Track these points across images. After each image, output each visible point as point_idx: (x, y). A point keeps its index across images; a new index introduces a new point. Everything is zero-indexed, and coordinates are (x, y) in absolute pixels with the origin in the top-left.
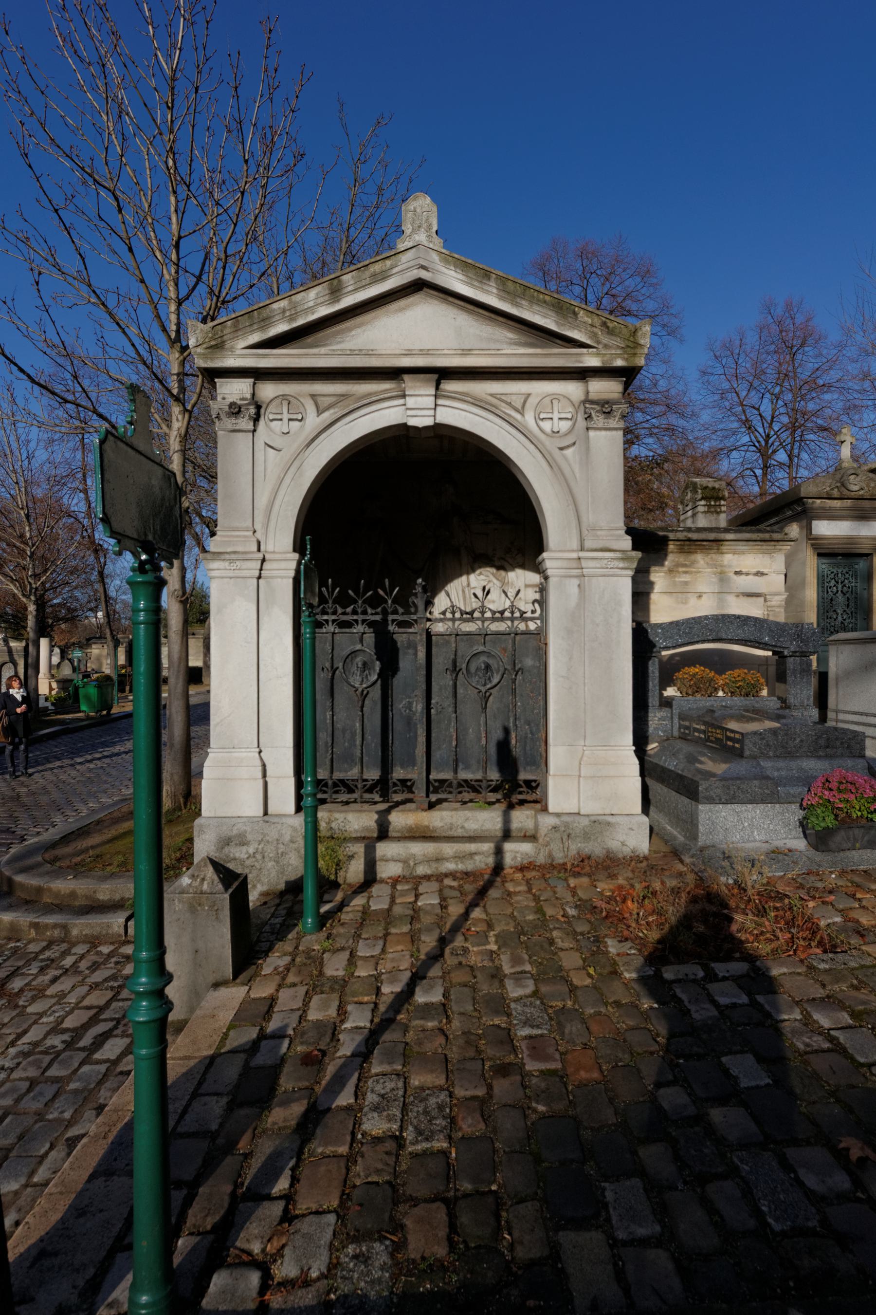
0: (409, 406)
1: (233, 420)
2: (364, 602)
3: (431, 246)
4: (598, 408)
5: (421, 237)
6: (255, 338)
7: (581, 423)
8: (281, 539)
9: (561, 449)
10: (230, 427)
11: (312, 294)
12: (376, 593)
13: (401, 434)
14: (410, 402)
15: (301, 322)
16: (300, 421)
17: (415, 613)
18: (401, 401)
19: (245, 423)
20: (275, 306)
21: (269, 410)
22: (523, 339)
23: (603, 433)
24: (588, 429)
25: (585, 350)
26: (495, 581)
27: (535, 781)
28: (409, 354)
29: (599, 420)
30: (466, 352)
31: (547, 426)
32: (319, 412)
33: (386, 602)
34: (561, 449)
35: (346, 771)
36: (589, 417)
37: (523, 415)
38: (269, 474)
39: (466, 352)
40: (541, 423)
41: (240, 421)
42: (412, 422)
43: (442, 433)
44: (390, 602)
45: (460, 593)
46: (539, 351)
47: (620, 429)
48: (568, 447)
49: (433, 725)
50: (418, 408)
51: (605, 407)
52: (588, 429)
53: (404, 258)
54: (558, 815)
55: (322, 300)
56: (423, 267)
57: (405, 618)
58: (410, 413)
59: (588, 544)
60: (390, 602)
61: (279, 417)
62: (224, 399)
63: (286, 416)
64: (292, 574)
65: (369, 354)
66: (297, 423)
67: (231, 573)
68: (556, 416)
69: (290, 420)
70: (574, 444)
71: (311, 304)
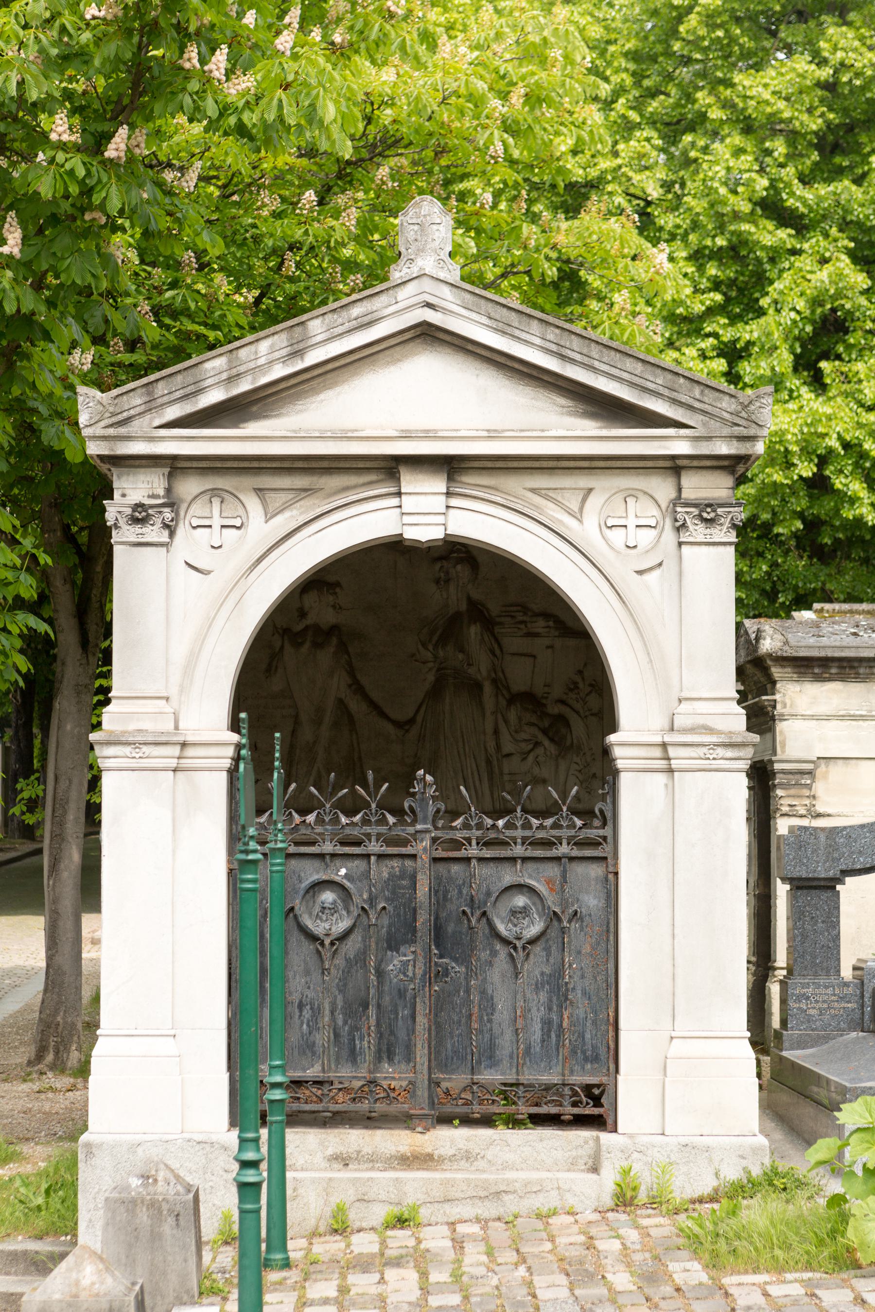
0: (405, 509)
1: (137, 529)
2: (334, 806)
3: (442, 275)
4: (695, 511)
5: (427, 263)
6: (173, 412)
7: (669, 536)
8: (208, 714)
9: (640, 573)
10: (133, 539)
11: (264, 347)
12: (353, 792)
13: (395, 548)
14: (408, 503)
15: (244, 386)
16: (238, 528)
17: (413, 824)
18: (395, 501)
19: (153, 533)
20: (208, 365)
21: (191, 512)
22: (590, 409)
23: (704, 549)
24: (680, 544)
25: (671, 431)
26: (546, 743)
27: (598, 1086)
28: (406, 436)
29: (698, 532)
30: (492, 435)
31: (617, 537)
32: (269, 517)
33: (368, 806)
34: (640, 573)
35: (304, 1070)
36: (680, 528)
37: (581, 521)
38: (189, 608)
39: (492, 435)
40: (608, 532)
41: (147, 529)
42: (411, 534)
43: (458, 553)
44: (374, 806)
45: (483, 764)
46: (605, 432)
47: (730, 544)
48: (651, 569)
49: (677, 809)
50: (423, 514)
51: (707, 511)
52: (680, 544)
53: (403, 294)
54: (631, 1136)
55: (277, 355)
56: (429, 305)
57: (399, 831)
58: (407, 519)
59: (679, 722)
60: (374, 806)
61: (206, 522)
62: (124, 495)
63: (217, 522)
64: (227, 763)
65: (429, 435)
66: (234, 530)
67: (133, 763)
68: (631, 522)
69: (223, 526)
70: (660, 564)
71: (262, 361)
